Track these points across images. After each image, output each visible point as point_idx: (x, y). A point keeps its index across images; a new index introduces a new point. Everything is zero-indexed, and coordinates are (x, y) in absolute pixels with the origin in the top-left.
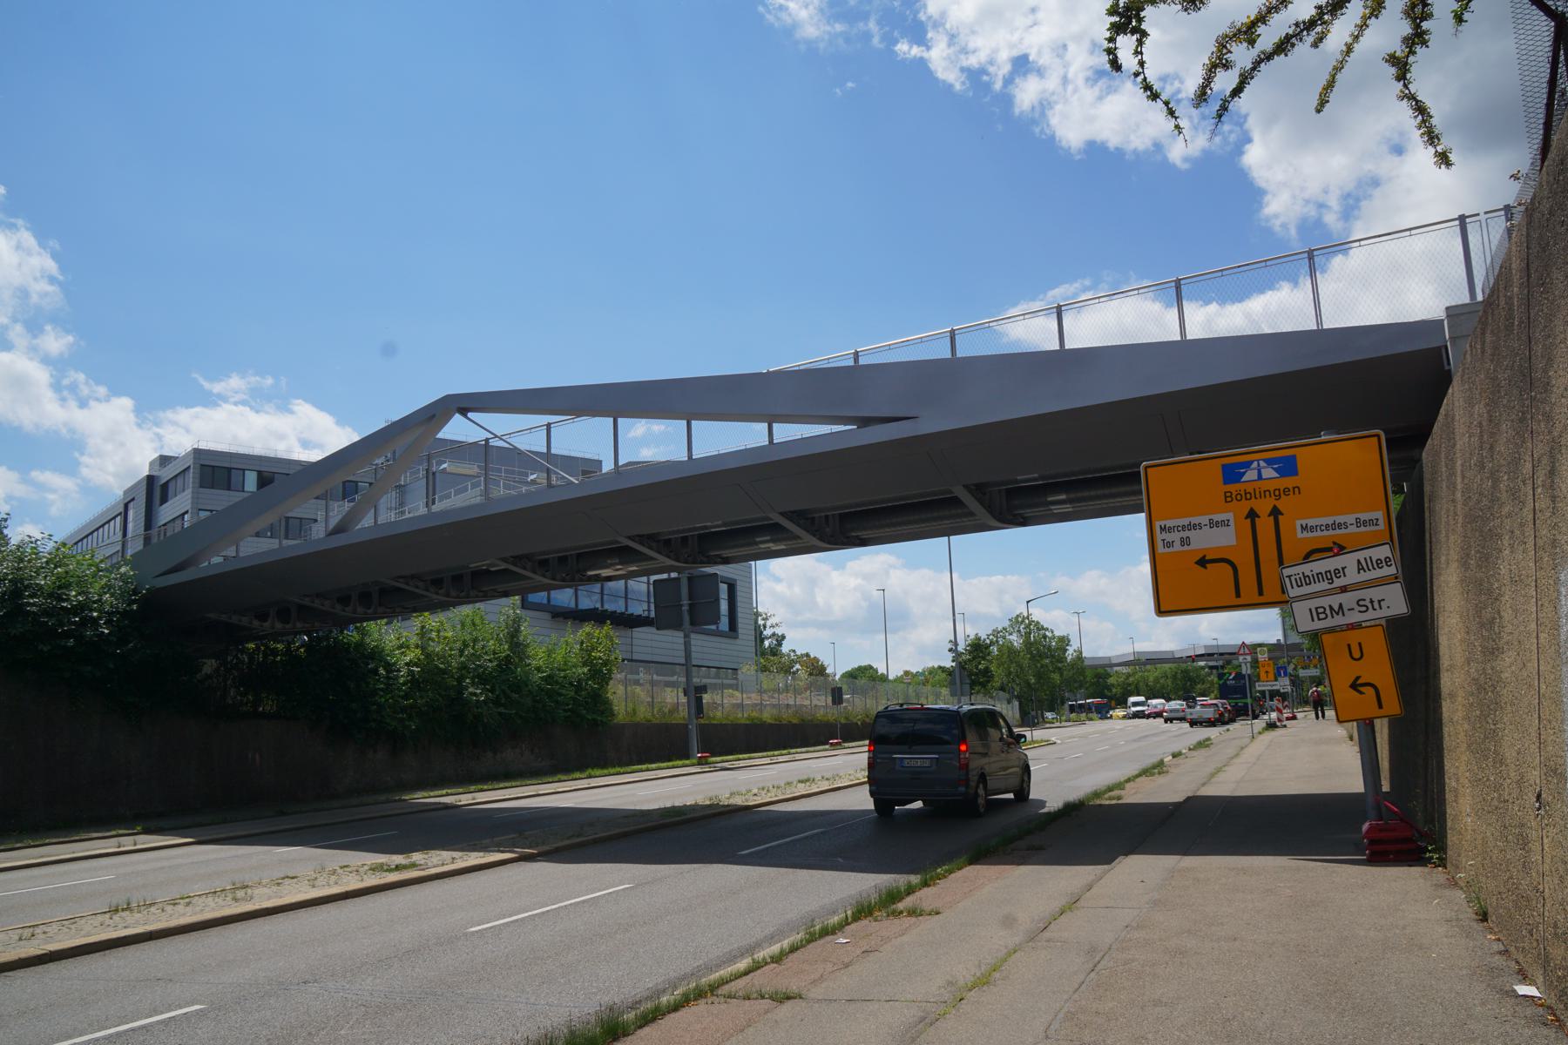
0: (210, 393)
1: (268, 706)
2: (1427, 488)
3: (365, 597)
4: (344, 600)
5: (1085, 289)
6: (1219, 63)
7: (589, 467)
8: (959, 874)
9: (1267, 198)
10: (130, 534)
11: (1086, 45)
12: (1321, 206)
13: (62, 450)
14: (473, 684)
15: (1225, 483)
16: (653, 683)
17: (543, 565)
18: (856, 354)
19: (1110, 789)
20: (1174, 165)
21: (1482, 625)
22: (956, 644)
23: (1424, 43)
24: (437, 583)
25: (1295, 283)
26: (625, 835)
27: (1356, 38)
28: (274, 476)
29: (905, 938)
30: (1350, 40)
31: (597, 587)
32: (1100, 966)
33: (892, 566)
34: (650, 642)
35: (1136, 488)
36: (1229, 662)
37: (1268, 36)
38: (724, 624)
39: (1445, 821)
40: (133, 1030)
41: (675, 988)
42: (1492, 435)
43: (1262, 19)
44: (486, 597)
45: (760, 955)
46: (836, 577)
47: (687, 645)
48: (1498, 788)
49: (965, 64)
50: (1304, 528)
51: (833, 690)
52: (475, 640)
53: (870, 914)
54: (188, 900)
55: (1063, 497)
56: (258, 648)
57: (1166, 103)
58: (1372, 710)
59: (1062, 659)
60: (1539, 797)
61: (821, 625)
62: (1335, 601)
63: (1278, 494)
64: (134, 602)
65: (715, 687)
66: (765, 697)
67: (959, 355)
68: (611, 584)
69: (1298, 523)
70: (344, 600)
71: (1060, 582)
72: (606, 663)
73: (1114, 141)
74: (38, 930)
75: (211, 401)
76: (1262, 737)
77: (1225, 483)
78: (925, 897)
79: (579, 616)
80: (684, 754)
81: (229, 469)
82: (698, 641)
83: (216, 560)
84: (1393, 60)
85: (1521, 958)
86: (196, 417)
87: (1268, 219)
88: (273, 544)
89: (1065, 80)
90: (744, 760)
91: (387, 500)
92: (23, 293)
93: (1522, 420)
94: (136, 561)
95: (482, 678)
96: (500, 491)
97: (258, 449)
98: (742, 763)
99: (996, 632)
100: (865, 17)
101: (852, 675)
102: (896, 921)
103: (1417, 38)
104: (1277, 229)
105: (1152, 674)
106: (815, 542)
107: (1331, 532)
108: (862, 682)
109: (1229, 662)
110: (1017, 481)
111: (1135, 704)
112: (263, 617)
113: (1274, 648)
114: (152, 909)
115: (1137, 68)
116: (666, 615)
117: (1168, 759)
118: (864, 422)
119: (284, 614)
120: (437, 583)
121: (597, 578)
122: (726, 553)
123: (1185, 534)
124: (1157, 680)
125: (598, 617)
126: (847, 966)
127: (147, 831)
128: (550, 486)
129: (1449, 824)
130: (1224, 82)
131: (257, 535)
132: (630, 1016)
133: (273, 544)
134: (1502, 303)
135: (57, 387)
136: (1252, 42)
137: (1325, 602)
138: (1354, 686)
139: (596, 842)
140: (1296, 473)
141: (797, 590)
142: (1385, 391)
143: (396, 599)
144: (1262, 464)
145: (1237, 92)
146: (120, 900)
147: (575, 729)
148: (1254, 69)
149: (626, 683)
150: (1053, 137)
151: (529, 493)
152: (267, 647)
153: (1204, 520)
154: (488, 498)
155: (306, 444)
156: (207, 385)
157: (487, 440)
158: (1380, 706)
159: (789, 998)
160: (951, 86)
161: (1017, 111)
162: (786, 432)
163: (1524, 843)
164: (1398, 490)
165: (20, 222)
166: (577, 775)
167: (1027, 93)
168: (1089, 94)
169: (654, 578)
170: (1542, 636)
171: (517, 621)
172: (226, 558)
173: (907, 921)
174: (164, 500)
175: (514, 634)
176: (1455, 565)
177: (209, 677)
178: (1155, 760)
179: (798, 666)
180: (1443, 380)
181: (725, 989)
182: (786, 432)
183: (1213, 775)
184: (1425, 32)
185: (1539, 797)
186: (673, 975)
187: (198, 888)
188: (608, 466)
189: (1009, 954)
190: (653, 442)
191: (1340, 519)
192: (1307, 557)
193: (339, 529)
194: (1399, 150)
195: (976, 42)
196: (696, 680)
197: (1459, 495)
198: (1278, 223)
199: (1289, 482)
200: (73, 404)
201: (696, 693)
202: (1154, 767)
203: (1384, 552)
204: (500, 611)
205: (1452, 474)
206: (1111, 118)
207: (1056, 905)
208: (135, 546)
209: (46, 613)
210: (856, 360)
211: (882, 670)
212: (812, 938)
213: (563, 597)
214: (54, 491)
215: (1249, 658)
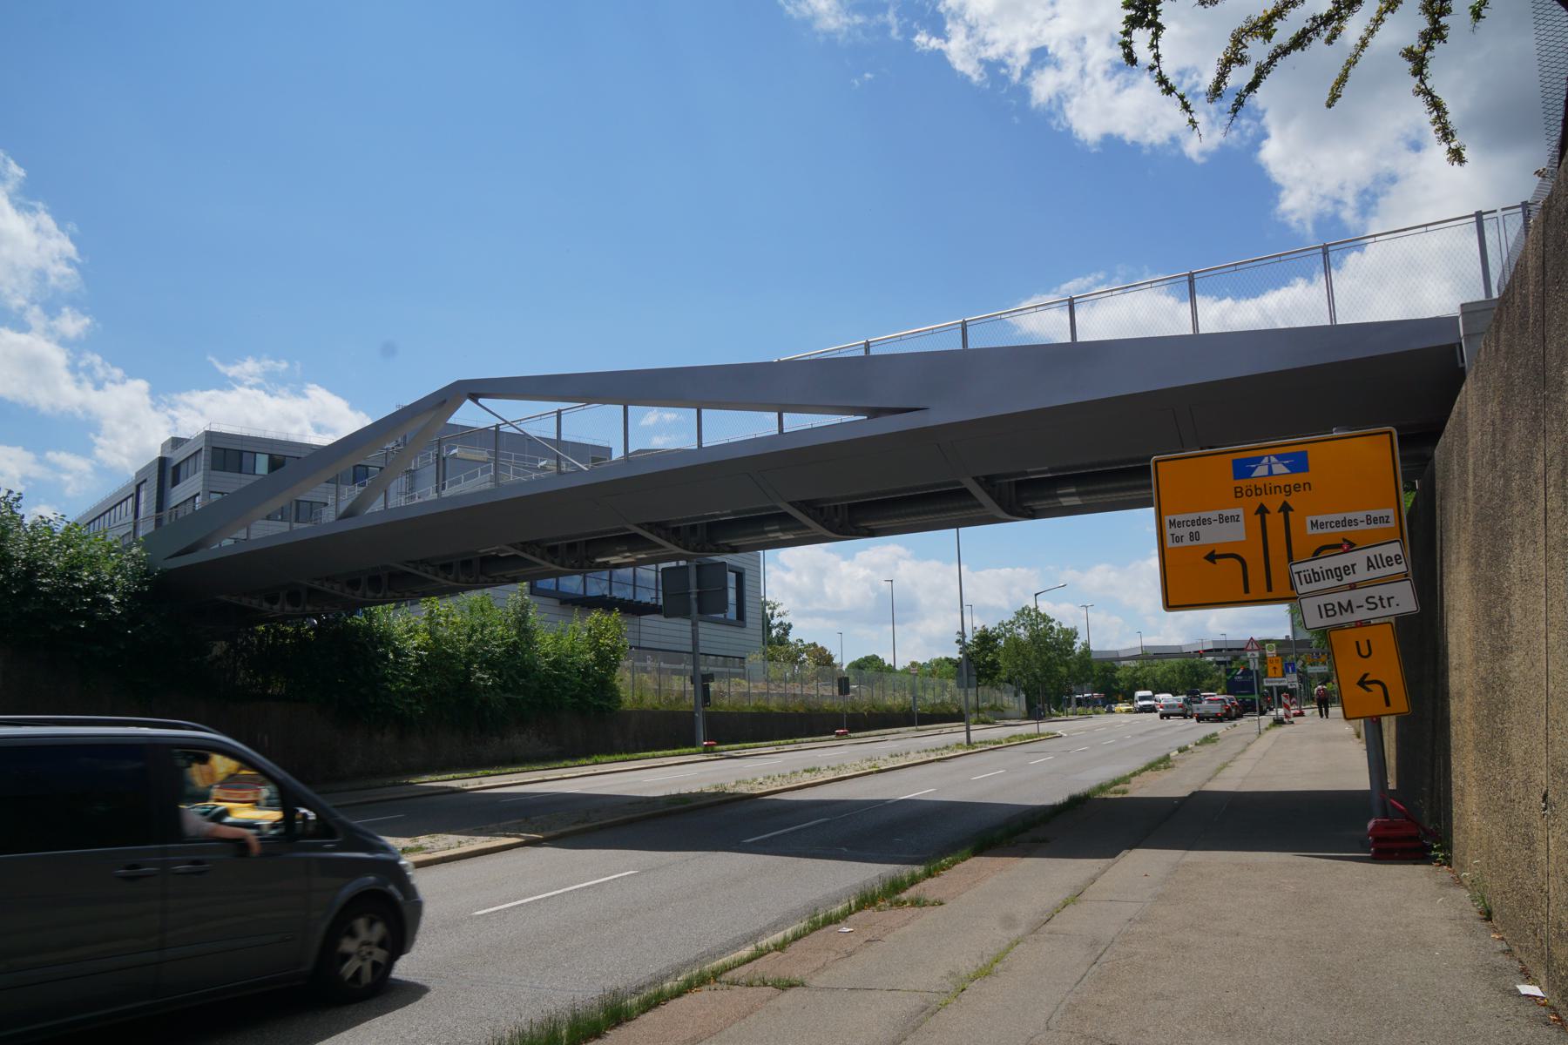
0: (225, 376)
1: (277, 688)
2: (1439, 486)
3: (375, 582)
4: (354, 584)
6: (1234, 58)
7: (599, 454)
9: (1284, 194)
10: (142, 515)
13: (77, 432)
14: (481, 669)
16: (660, 671)
18: (867, 345)
19: (1115, 783)
20: (1191, 160)
21: (1492, 624)
23: (1442, 38)
24: (446, 568)
26: (630, 822)
28: (286, 460)
29: (908, 928)
30: (1364, 34)
31: (605, 574)
32: (1102, 959)
34: (658, 629)
35: (1145, 482)
37: (1284, 31)
41: (679, 974)
42: (1505, 433)
44: (495, 582)
45: (763, 943)
46: (845, 567)
48: (1504, 787)
49: (983, 55)
50: (1314, 525)
51: (840, 680)
52: (484, 626)
53: (874, 903)
56: (267, 630)
57: (1182, 97)
60: (1545, 797)
61: (828, 615)
62: (1343, 598)
63: (1288, 490)
64: (146, 583)
65: (721, 675)
70: (354, 584)
71: (1069, 575)
72: (614, 650)
73: (1130, 135)
75: (225, 384)
76: (1268, 733)
78: (930, 888)
79: (587, 603)
80: (689, 742)
81: (241, 452)
82: (705, 629)
83: (227, 542)
84: (1409, 54)
85: (1524, 957)
87: (1284, 215)
88: (283, 527)
91: (398, 485)
92: (41, 275)
93: (1535, 419)
94: (148, 543)
95: (490, 664)
96: (510, 477)
101: (859, 666)
102: (900, 911)
103: (1435, 33)
104: (1294, 224)
105: (1160, 668)
106: (817, 528)
107: (1341, 529)
108: (868, 672)
109: (1236, 658)
110: (1027, 474)
111: (1142, 698)
112: (273, 600)
113: (1282, 644)
115: (1152, 61)
116: (674, 602)
117: (1174, 754)
118: (875, 413)
119: (294, 597)
120: (446, 568)
121: (606, 566)
122: (735, 542)
123: (1194, 529)
124: (1164, 675)
125: (605, 604)
126: (849, 955)
128: (560, 472)
129: (1455, 822)
130: (1239, 77)
131: (268, 518)
133: (283, 527)
135: (73, 369)
136: (1268, 37)
138: (1363, 683)
139: (602, 828)
141: (805, 579)
142: (1397, 388)
143: (405, 584)
144: (1273, 459)
145: (1253, 86)
147: (583, 715)
148: (1270, 63)
149: (633, 670)
151: (539, 480)
152: (277, 630)
153: (1214, 515)
154: (497, 484)
156: (222, 368)
157: (497, 426)
158: (1388, 704)
160: (969, 77)
161: (1034, 103)
162: (796, 422)
163: (1529, 842)
165: (40, 205)
166: (584, 761)
167: (1044, 86)
170: (1551, 635)
171: (525, 607)
172: (236, 541)
173: (910, 912)
174: (176, 482)
175: (521, 622)
176: (1465, 563)
177: (218, 658)
178: (1161, 755)
180: (1456, 377)
181: (729, 976)
182: (796, 422)
183: (1219, 770)
184: (1445, 27)
185: (1545, 797)
186: (676, 961)
188: (618, 454)
189: (1011, 946)
190: (663, 430)
191: (1350, 516)
192: (1317, 554)
193: (349, 514)
194: (1416, 146)
195: (994, 34)
196: (703, 669)
197: (1470, 493)
198: (1294, 218)
199: (1300, 478)
200: (88, 386)
202: (1160, 761)
203: (1394, 549)
204: (512, 596)
205: (1464, 472)
207: (1059, 898)
208: (146, 528)
211: (888, 661)
212: (815, 927)
213: (572, 584)
214: (69, 472)
215: (1257, 654)
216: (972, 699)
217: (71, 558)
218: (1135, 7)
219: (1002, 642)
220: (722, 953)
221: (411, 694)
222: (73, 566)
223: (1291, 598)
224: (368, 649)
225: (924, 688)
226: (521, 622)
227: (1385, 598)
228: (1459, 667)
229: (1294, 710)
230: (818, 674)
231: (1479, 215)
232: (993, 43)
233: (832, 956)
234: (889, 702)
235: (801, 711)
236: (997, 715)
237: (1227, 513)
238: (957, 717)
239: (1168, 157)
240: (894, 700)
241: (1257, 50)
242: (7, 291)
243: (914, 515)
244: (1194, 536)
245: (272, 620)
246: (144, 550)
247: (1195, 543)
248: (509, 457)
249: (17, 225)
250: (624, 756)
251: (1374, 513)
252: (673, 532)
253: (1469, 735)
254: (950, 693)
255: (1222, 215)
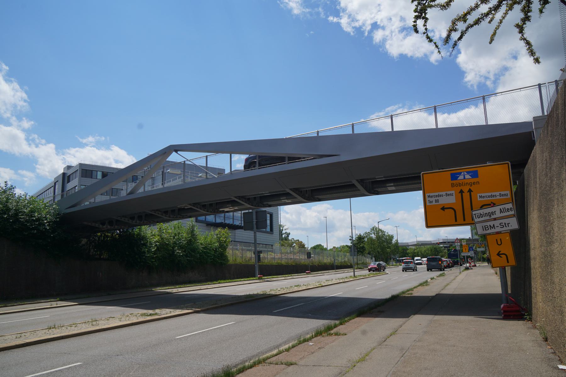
1: (105, 256)
2: (526, 183)
3: (140, 218)
4: (132, 218)
5: (399, 108)
6: (452, 29)
7: (220, 172)
8: (353, 321)
9: (466, 75)
10: (56, 194)
11: (399, 18)
12: (486, 78)
13: (29, 162)
14: (178, 249)
15: (452, 180)
16: (242, 250)
17: (204, 207)
18: (318, 132)
19: (408, 291)
21: (546, 233)
22: (352, 237)
23: (529, 20)
24: (166, 212)
25: (476, 106)
26: (232, 304)
27: (504, 18)
28: (108, 174)
29: (334, 344)
30: (501, 19)
31: (223, 215)
32: (405, 355)
33: (328, 209)
34: (241, 234)
35: (419, 181)
36: (451, 245)
37: (471, 19)
38: (268, 229)
39: (532, 304)
40: (56, 371)
41: (251, 360)
42: (551, 164)
43: (468, 13)
44: (183, 217)
46: (308, 212)
47: (255, 236)
48: (552, 292)
49: (353, 25)
50: (480, 197)
51: (307, 253)
52: (179, 233)
53: (321, 334)
54: (76, 325)
55: (392, 184)
56: (101, 235)
57: (435, 43)
58: (504, 263)
59: (391, 243)
61: (303, 229)
62: (491, 223)
63: (471, 184)
64: (58, 218)
66: (283, 255)
67: (355, 132)
68: (227, 214)
69: (478, 195)
70: (132, 218)
71: (390, 215)
72: (225, 242)
73: (410, 54)
74: (23, 335)
75: (82, 146)
76: (463, 273)
77: (452, 180)
81: (92, 171)
82: (259, 235)
83: (87, 203)
84: (517, 26)
85: (560, 355)
86: (77, 151)
87: (466, 83)
88: (107, 198)
89: (392, 32)
90: (275, 278)
91: (149, 182)
92: (15, 106)
95: (181, 247)
96: (188, 180)
97: (99, 163)
98: (274, 279)
99: (366, 233)
100: (318, 6)
101: (315, 248)
102: (331, 337)
103: (527, 18)
104: (469, 86)
105: (423, 249)
107: (490, 198)
108: (317, 250)
109: (451, 245)
110: (375, 178)
111: (417, 260)
112: (103, 224)
113: (468, 240)
114: (63, 328)
115: (424, 31)
116: (247, 225)
117: (429, 280)
119: (111, 223)
120: (166, 212)
121: (223, 212)
122: (270, 203)
123: (437, 198)
124: (425, 251)
125: (223, 225)
126: (313, 353)
127: (61, 300)
128: (207, 178)
129: (533, 305)
130: (455, 36)
131: (102, 195)
132: (234, 370)
133: (107, 198)
134: (555, 116)
135: (27, 139)
137: (488, 224)
139: (221, 306)
140: (477, 177)
141: (294, 216)
142: (510, 147)
143: (151, 218)
144: (465, 173)
145: (460, 38)
146: (52, 324)
147: (215, 266)
148: (466, 30)
149: (233, 249)
150: (387, 52)
152: (105, 235)
153: (444, 193)
155: (117, 162)
156: (81, 140)
157: (184, 161)
158: (508, 262)
159: (292, 364)
160: (349, 33)
161: (374, 43)
164: (515, 183)
165: (13, 79)
166: (215, 282)
167: (378, 36)
168: (401, 36)
169: (243, 212)
171: (193, 227)
173: (334, 337)
174: (69, 182)
175: (192, 232)
177: (84, 245)
178: (424, 280)
179: (295, 244)
180: (532, 144)
181: (269, 361)
183: (446, 286)
184: (530, 16)
186: (249, 355)
187: (79, 321)
188: (227, 171)
189: (372, 350)
191: (494, 194)
192: (482, 207)
193: (131, 193)
194: (515, 58)
195: (359, 17)
196: (258, 249)
198: (470, 84)
199: (475, 180)
200: (33, 146)
201: (258, 254)
202: (424, 283)
203: (510, 206)
204: (189, 222)
205: (535, 178)
206: (413, 46)
207: (389, 333)
208: (58, 198)
209: (27, 221)
210: (318, 133)
211: (325, 247)
212: (300, 343)
213: (211, 218)
214: (27, 177)
215: (459, 244)
216: (355, 260)
217: (32, 208)
218: (418, 12)
219: (366, 239)
220: (266, 352)
221: (153, 258)
222: (32, 211)
223: (471, 223)
224: (141, 241)
225: (338, 256)
226: (192, 232)
227: (506, 223)
228: (534, 249)
229: (473, 264)
230: (300, 251)
231: (539, 85)
232: (357, 21)
233: (306, 354)
234: (325, 261)
235: (293, 264)
236: (364, 266)
237: (449, 192)
238: (350, 267)
239: (422, 62)
240: (327, 260)
241: (461, 26)
242: (2, 112)
243: (335, 193)
244: (437, 201)
245: (104, 231)
246: (58, 206)
247: (437, 203)
248: (188, 172)
249: (6, 87)
250: (230, 281)
251: (502, 193)
252: (248, 200)
253: (538, 273)
254: (347, 258)
255: (442, 82)
